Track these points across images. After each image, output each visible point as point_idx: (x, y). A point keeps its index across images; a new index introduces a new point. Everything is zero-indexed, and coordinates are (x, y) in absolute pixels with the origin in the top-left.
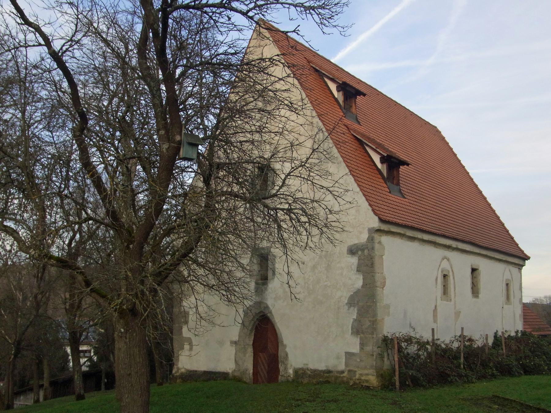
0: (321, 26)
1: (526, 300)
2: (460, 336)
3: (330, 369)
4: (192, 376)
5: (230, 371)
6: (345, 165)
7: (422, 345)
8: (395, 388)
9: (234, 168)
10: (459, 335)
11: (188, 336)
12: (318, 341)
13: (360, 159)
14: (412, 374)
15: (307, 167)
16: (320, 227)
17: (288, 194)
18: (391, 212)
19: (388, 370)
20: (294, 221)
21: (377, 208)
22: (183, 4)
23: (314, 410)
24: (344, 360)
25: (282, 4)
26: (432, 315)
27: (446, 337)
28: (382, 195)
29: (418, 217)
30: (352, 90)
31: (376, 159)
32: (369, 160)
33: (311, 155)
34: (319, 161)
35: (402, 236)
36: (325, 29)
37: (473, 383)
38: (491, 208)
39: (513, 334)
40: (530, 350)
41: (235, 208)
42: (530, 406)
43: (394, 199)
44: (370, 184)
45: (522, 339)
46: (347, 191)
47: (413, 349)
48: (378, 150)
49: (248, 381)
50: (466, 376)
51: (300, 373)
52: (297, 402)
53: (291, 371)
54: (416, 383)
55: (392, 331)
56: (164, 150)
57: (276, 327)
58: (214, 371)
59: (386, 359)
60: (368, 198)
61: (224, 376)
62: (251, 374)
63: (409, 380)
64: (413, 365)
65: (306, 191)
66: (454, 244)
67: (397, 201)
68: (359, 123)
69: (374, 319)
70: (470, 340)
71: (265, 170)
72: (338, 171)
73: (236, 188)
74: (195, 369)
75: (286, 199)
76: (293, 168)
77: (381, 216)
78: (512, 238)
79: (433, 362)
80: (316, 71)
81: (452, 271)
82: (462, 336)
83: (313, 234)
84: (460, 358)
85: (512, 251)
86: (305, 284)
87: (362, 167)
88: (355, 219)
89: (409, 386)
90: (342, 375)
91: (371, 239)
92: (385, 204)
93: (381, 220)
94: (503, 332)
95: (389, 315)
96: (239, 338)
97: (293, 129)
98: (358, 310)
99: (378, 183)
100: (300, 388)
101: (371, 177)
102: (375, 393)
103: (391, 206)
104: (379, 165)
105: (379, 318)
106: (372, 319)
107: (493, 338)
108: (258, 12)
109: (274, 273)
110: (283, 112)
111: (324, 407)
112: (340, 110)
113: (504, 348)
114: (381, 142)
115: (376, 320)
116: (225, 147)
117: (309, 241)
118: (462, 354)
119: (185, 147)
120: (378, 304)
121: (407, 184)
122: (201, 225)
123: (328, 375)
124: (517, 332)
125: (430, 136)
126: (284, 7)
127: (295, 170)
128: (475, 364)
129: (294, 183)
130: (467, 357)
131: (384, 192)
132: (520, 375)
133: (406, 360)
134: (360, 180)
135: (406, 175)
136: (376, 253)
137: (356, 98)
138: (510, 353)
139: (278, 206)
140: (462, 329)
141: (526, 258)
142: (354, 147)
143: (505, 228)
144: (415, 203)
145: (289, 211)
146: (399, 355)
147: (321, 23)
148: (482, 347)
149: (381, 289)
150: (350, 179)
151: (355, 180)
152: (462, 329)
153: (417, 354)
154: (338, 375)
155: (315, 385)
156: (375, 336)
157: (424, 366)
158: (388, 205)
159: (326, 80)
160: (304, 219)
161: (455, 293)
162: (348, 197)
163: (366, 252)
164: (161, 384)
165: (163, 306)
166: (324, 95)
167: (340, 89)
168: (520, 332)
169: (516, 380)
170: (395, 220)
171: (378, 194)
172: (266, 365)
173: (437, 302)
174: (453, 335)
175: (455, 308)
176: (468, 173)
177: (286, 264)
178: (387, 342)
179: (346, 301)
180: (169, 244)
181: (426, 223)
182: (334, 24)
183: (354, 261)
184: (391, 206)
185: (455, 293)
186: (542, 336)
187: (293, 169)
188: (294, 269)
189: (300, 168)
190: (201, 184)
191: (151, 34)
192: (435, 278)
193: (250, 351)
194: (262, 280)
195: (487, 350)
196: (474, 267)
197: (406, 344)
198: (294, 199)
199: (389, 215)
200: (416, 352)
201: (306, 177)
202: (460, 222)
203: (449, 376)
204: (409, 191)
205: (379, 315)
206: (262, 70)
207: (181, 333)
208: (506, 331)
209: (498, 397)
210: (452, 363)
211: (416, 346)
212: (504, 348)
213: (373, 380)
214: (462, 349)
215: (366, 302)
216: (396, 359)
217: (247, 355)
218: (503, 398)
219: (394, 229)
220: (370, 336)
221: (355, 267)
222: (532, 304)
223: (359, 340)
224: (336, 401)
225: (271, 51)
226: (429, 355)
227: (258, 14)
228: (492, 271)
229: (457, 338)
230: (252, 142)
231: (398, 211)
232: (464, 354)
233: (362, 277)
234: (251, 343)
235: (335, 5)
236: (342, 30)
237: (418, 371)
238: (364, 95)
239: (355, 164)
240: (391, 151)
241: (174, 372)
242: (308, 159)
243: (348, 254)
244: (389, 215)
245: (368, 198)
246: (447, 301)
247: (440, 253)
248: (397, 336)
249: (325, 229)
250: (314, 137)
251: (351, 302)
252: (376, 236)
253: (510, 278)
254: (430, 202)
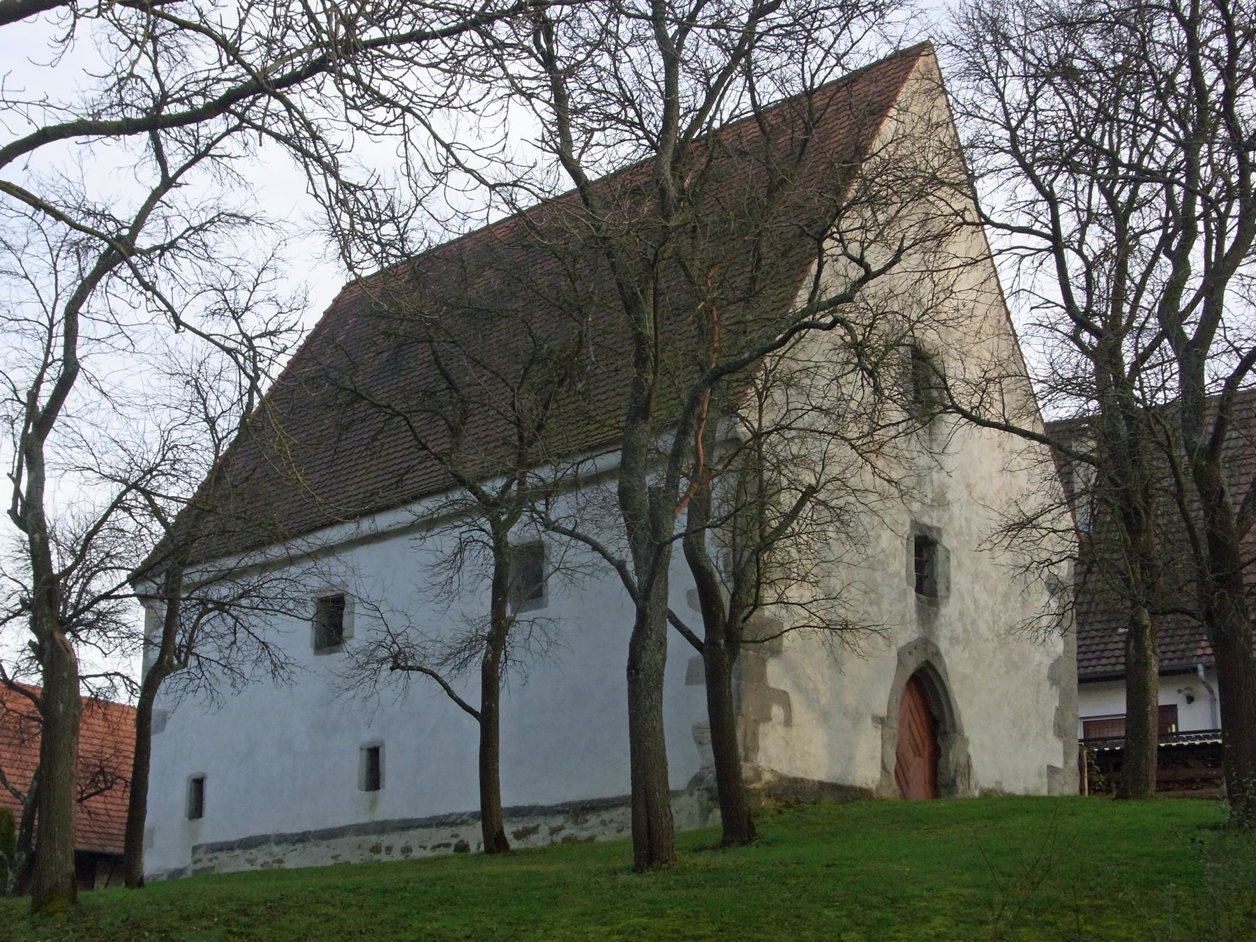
5: (873, 786)
11: (783, 687)
51: (986, 794)
58: (840, 782)
74: (801, 775)
125: (331, 652)
196: (197, 776)
207: (762, 677)
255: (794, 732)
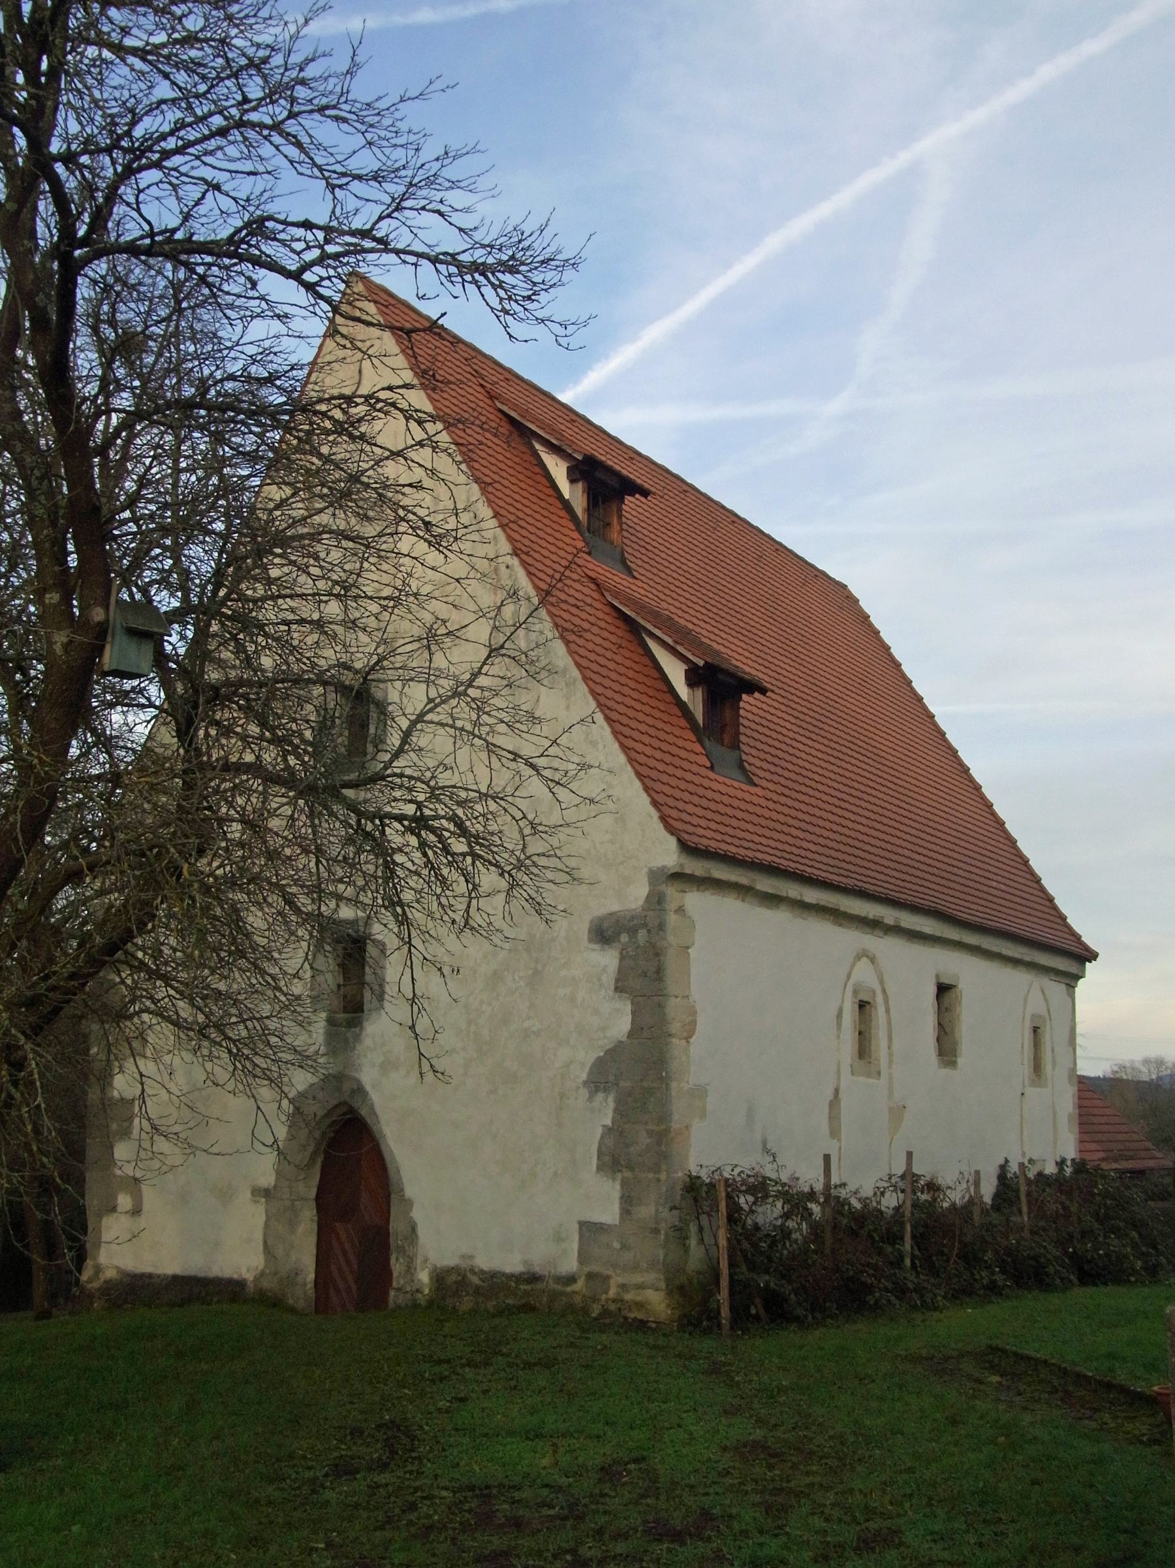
0: (502, 319)
1: (1092, 1066)
2: (903, 1177)
3: (537, 1269)
4: (137, 1290)
5: (249, 1277)
6: (586, 689)
7: (796, 1202)
8: (719, 1325)
9: (262, 697)
10: (900, 1174)
12: (501, 1188)
13: (631, 674)
14: (767, 1283)
15: (473, 700)
16: (508, 868)
17: (415, 775)
18: (713, 826)
19: (699, 1273)
20: (430, 853)
21: (674, 813)
22: (122, 239)
23: (485, 1392)
24: (575, 1246)
25: (397, 252)
26: (827, 1115)
27: (865, 1179)
28: (688, 776)
29: (790, 840)
30: (612, 478)
31: (676, 673)
32: (657, 675)
33: (484, 663)
34: (505, 682)
35: (743, 891)
36: (516, 328)
37: (936, 1309)
38: (994, 814)
39: (1050, 1169)
40: (1096, 1216)
41: (265, 812)
42: (1085, 1377)
43: (723, 789)
44: (656, 743)
45: (1077, 1181)
46: (584, 767)
47: (770, 1213)
48: (679, 648)
49: (301, 1304)
50: (919, 1290)
51: (451, 1283)
52: (437, 1369)
53: (424, 1277)
54: (777, 1312)
55: (712, 1162)
56: (58, 649)
57: (384, 1148)
59: (693, 1242)
60: (649, 783)
61: (231, 1290)
62: (310, 1285)
63: (758, 1301)
64: (770, 1260)
65: (470, 769)
66: (888, 915)
67: (731, 791)
68: (629, 571)
69: (663, 1127)
70: (932, 1187)
71: (360, 700)
72: (568, 707)
73: (269, 756)
74: (149, 1269)
75: (410, 790)
76: (430, 701)
77: (686, 837)
78: (1051, 900)
79: (827, 1251)
80: (512, 421)
81: (884, 991)
82: (910, 1177)
83: (485, 887)
84: (902, 1238)
85: (1047, 936)
86: (469, 1023)
87: (635, 695)
88: (612, 842)
89: (757, 1318)
90: (569, 1289)
91: (656, 900)
92: (696, 800)
93: (686, 847)
94: (1021, 1165)
95: (703, 1115)
96: (277, 1180)
97: (441, 590)
98: (618, 1102)
99: (680, 743)
100: (448, 1327)
101: (660, 725)
102: (661, 1341)
103: (713, 806)
104: (683, 691)
105: (675, 1126)
106: (655, 1128)
107: (995, 1182)
108: (332, 272)
109: (381, 997)
110: (406, 544)
111: (513, 1383)
112: (576, 535)
113: (1025, 1209)
114: (690, 626)
115: (667, 1130)
116: (241, 636)
117: (472, 911)
118: (908, 1228)
119: (117, 637)
120: (674, 1085)
121: (760, 746)
122: (170, 853)
123: (528, 1287)
124: (1061, 1163)
126: (404, 262)
127: (436, 706)
128: (943, 1254)
129: (435, 742)
130: (922, 1235)
131: (695, 768)
132: (1067, 1285)
133: (750, 1246)
134: (626, 731)
135: (757, 719)
136: (671, 939)
137: (623, 502)
138: (1042, 1224)
139: (388, 809)
140: (910, 1155)
141: (1086, 955)
142: (613, 638)
143: (1032, 873)
144: (783, 800)
145: (418, 824)
146: (730, 1230)
147: (507, 312)
148: (965, 1207)
149: (684, 1042)
150: (602, 730)
151: (615, 733)
152: (910, 1155)
153: (782, 1228)
154: (559, 1287)
155: (494, 1316)
156: (663, 1176)
157: (792, 1272)
158: (704, 803)
159: (538, 446)
160: (459, 846)
161: (891, 1055)
162: (589, 785)
163: (642, 935)
164: (45, 1315)
165: (39, 1099)
166: (532, 490)
167: (577, 476)
168: (1069, 1163)
169: (1055, 1299)
170: (724, 847)
171: (679, 773)
172: (352, 1257)
173: (839, 1078)
174: (884, 1174)
175: (891, 1092)
176: (932, 717)
177: (408, 970)
178: (697, 1192)
179: (584, 1076)
180: (73, 908)
181: (810, 855)
182: (540, 314)
183: (608, 960)
184: (713, 806)
185: (891, 1055)
186: (1132, 1172)
187: (433, 704)
188: (430, 983)
189: (454, 702)
190: (168, 737)
191: (27, 324)
192: (835, 1012)
193: (308, 1218)
194: (345, 1010)
195: (977, 1218)
196: (945, 980)
197: (751, 1199)
198: (433, 789)
199: (709, 833)
200: (779, 1222)
201: (469, 727)
202: (906, 853)
203: (869, 1289)
204: (765, 765)
205: (676, 1117)
206: (346, 429)
207: (111, 1161)
208: (1031, 1161)
209: (1003, 1351)
210: (880, 1252)
211: (779, 1204)
212: (1025, 1209)
213: (657, 1303)
214: (908, 1214)
215: (639, 1077)
216: (723, 1242)
217: (301, 1229)
218: (1015, 1354)
219: (721, 872)
220: (651, 1175)
221: (609, 979)
222: (1111, 1079)
223: (618, 1187)
224: (548, 1364)
225: (385, 367)
226: (816, 1228)
227: (329, 278)
228: (994, 992)
229: (893, 1181)
230: (319, 625)
231: (734, 822)
232: (914, 1227)
233: (628, 1008)
234: (313, 1192)
235: (543, 262)
236: (560, 331)
237: (783, 1277)
238: (645, 493)
239: (616, 687)
240: (718, 653)
241: (84, 1277)
242: (475, 675)
243: (590, 940)
244: (709, 833)
245: (649, 783)
246: (869, 1075)
247: (853, 939)
248: (726, 1175)
249: (520, 876)
250: (493, 614)
251: (601, 1077)
252: (671, 892)
253: (1045, 1013)
254: (825, 798)
255: (142, 1221)
